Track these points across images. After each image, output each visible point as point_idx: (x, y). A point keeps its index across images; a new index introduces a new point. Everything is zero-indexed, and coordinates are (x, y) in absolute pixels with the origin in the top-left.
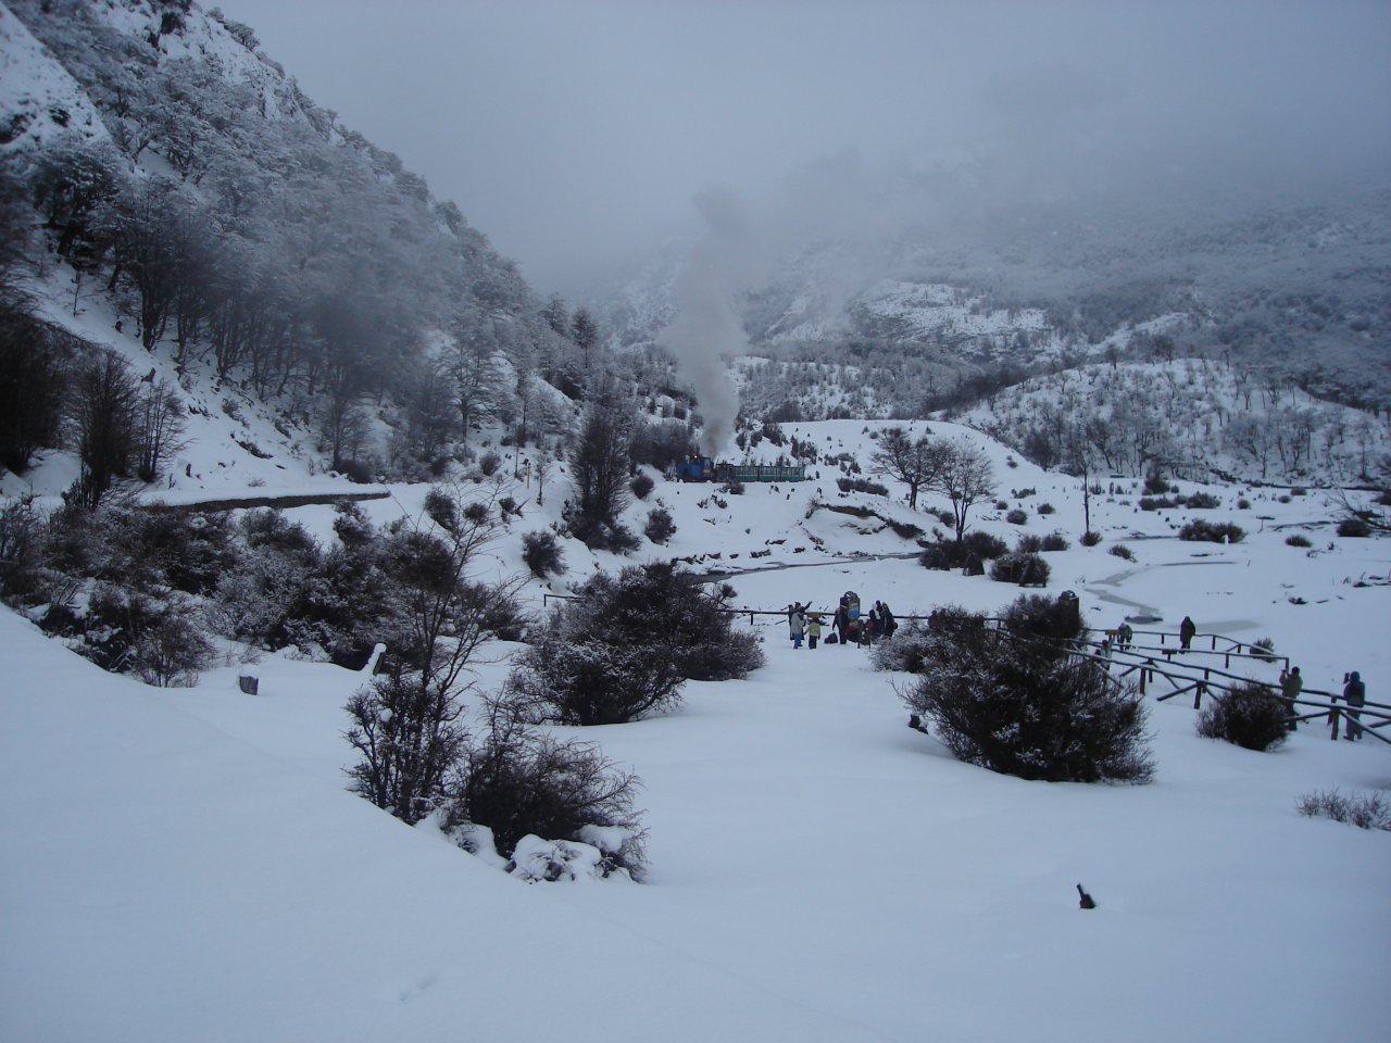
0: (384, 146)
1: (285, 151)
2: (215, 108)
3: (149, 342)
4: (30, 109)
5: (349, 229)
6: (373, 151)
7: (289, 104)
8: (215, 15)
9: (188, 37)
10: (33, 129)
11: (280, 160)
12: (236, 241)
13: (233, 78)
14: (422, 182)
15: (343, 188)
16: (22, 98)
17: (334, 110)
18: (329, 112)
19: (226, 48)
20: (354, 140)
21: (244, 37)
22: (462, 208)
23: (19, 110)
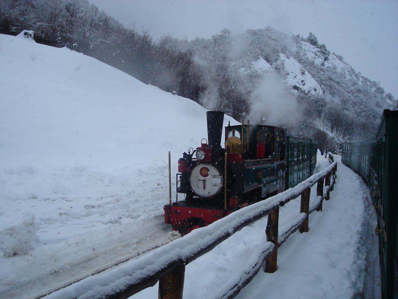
0: (372, 80)
1: (352, 88)
2: (337, 80)
3: (332, 132)
4: (311, 89)
5: (367, 107)
6: (370, 81)
7: (351, 74)
8: (334, 54)
9: (329, 61)
10: (311, 93)
11: (351, 91)
12: (345, 112)
13: (339, 70)
14: (383, 89)
15: (365, 96)
16: (309, 87)
17: (360, 72)
18: (359, 72)
19: (337, 63)
20: (365, 80)
21: (340, 58)
22: (393, 95)
23: (309, 90)
